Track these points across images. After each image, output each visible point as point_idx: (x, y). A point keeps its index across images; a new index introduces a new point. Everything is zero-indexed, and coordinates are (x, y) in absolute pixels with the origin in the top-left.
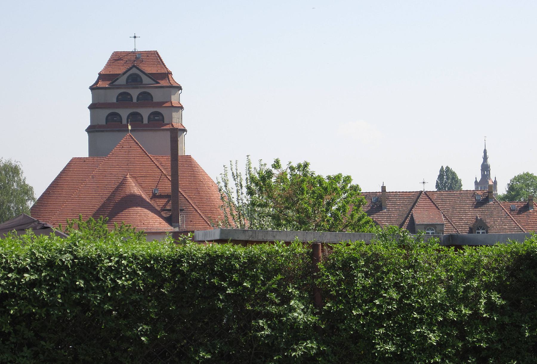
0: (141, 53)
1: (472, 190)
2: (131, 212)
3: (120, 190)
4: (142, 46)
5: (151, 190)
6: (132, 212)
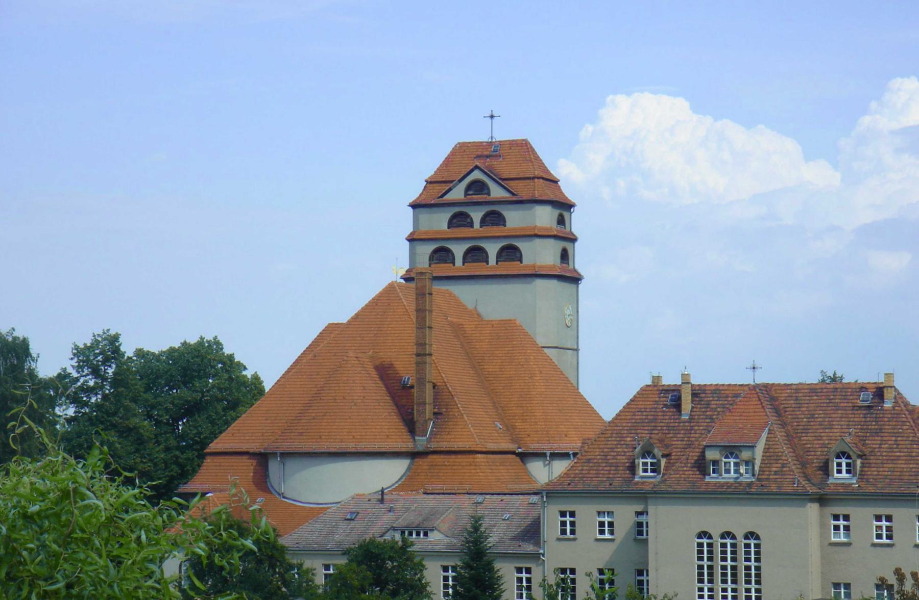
0: (501, 143)
1: (678, 384)
4: (504, 133)
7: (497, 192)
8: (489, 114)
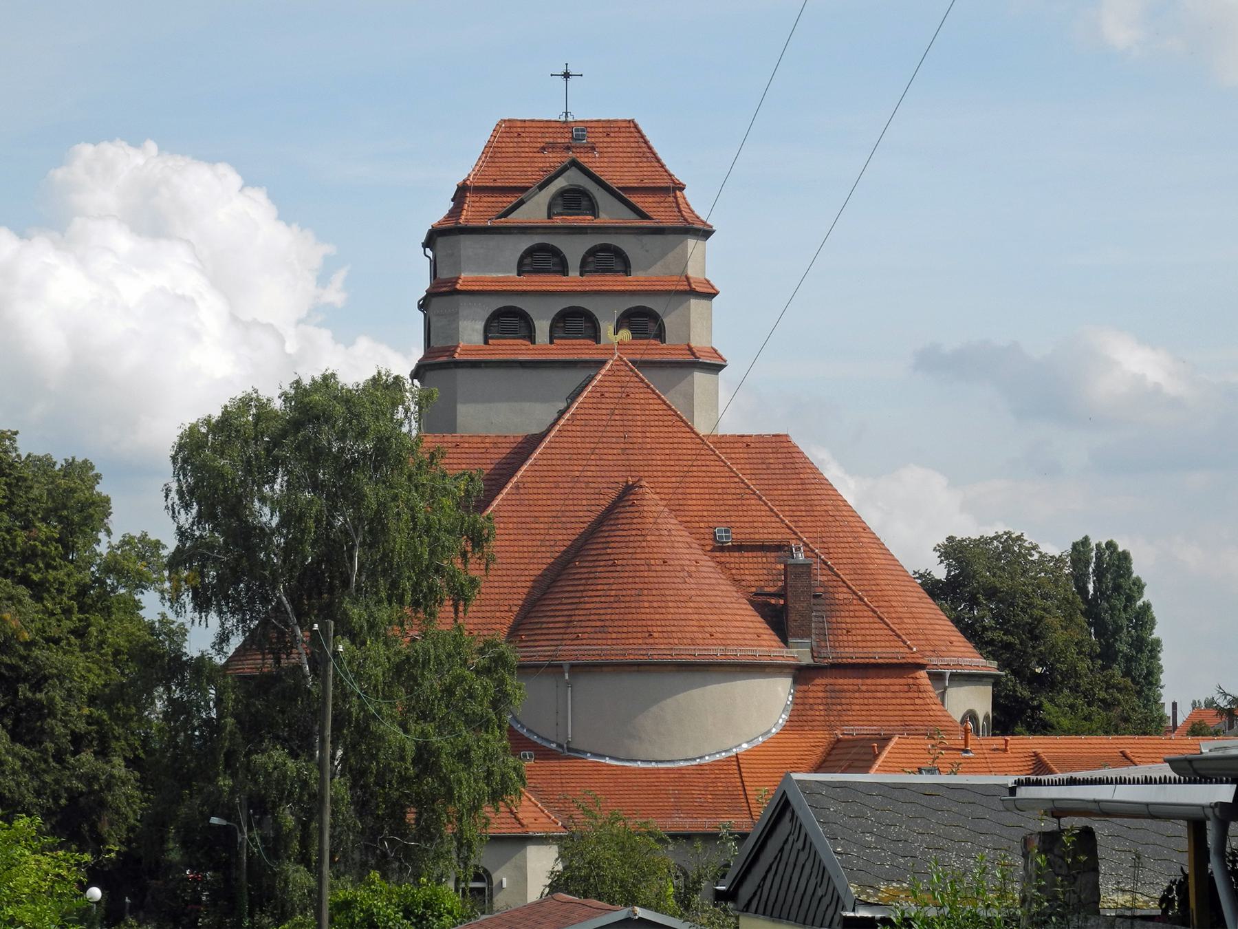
0: (586, 127)
2: (668, 598)
3: (606, 534)
5: (707, 530)
6: (673, 598)
7: (610, 213)
8: (562, 70)
